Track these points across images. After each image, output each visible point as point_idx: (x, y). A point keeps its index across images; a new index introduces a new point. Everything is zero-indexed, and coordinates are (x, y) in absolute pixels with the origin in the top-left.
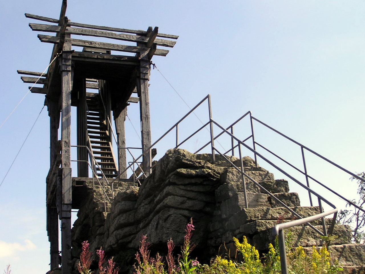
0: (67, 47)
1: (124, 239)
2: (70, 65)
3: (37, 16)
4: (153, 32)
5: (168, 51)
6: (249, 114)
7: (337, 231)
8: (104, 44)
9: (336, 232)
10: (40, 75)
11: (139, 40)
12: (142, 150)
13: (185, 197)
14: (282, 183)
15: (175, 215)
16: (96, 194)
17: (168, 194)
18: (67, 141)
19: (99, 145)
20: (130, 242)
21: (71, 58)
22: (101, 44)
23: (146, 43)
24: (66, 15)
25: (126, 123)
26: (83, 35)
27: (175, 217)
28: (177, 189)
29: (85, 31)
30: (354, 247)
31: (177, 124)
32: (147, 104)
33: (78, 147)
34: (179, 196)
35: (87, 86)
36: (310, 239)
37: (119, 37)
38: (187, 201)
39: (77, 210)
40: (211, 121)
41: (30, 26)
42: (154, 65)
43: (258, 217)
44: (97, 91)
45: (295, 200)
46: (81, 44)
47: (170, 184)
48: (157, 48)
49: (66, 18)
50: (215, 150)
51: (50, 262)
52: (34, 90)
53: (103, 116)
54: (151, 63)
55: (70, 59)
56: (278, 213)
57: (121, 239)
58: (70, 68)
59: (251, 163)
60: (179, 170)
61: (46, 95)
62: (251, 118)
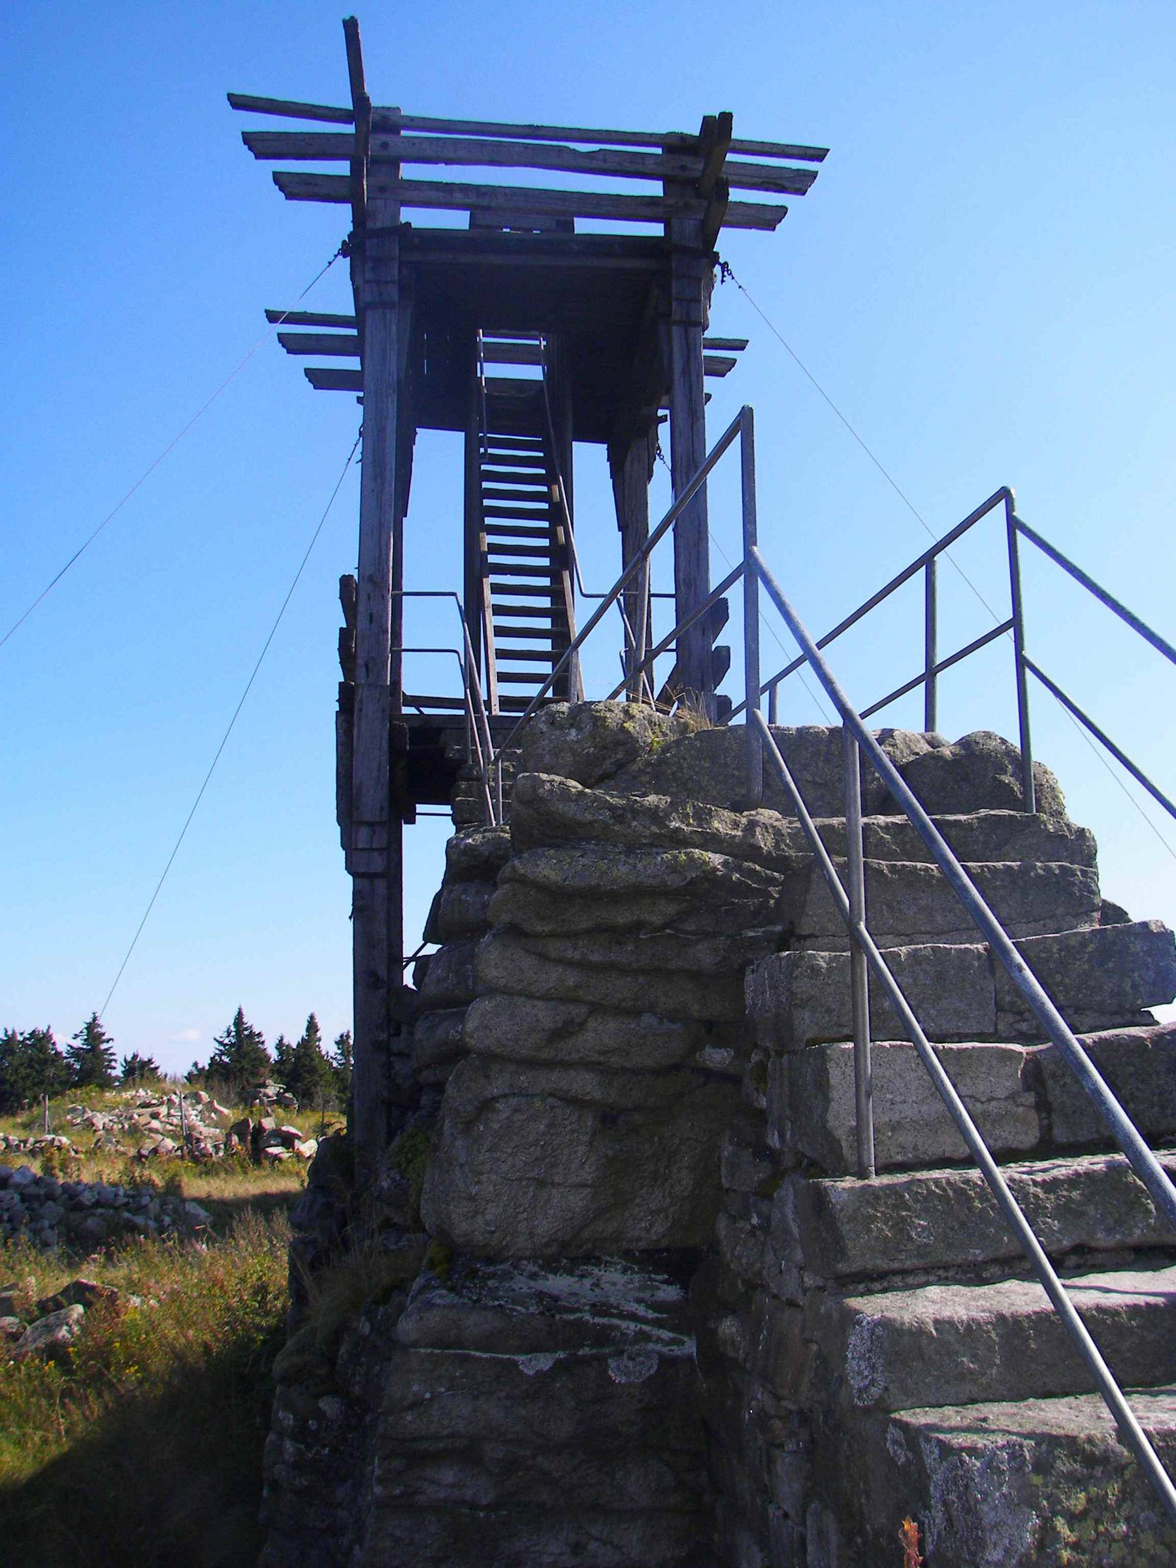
2: (392, 282)
5: (782, 211)
12: (674, 599)
13: (576, 1001)
14: (1137, 947)
15: (514, 1101)
26: (448, 162)
28: (528, 963)
34: (538, 998)
42: (724, 266)
48: (731, 198)
52: (320, 379)
62: (1014, 525)
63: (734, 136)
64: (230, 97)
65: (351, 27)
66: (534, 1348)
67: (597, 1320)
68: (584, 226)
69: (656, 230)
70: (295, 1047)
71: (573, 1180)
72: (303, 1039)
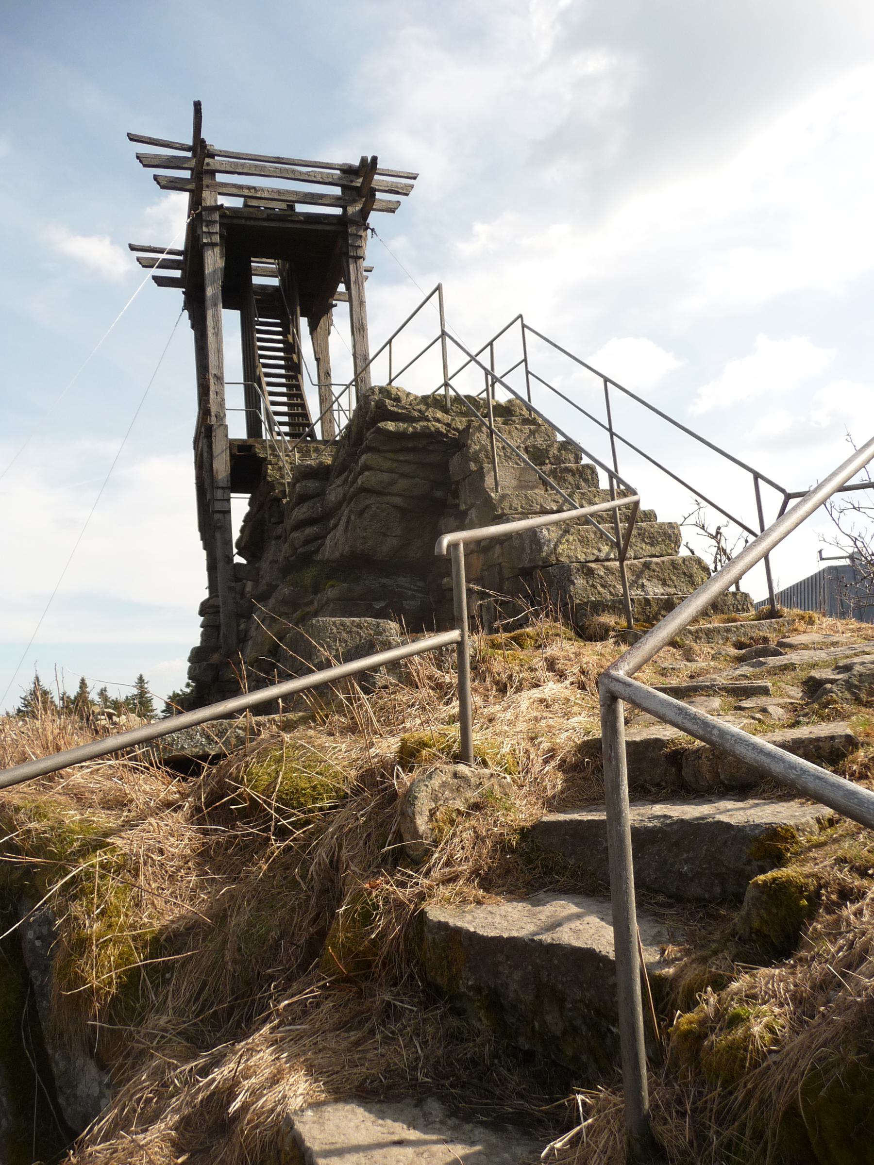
0: (209, 198)
1: (306, 547)
2: (217, 233)
3: (150, 138)
4: (369, 167)
6: (520, 320)
7: (655, 534)
8: (279, 192)
9: (652, 536)
10: (161, 251)
11: (344, 182)
15: (377, 505)
16: (273, 467)
17: (366, 468)
18: (219, 374)
19: (283, 380)
20: (317, 551)
21: (218, 218)
22: (273, 191)
23: (357, 187)
24: (203, 135)
25: (332, 339)
26: (239, 174)
27: (378, 508)
29: (243, 165)
30: (680, 562)
31: (390, 342)
32: (362, 303)
33: (245, 385)
35: (253, 272)
36: (602, 547)
37: (306, 178)
38: (400, 481)
39: (249, 495)
40: (444, 334)
41: (138, 158)
42: (373, 230)
43: (515, 508)
44: (275, 282)
45: (590, 477)
46: (235, 191)
47: (369, 449)
49: (203, 141)
50: (450, 389)
51: (206, 584)
52: (161, 281)
53: (288, 327)
54: (367, 228)
55: (216, 222)
56: (554, 501)
57: (301, 547)
58: (217, 239)
59: (522, 409)
60: (381, 425)
61: (184, 290)
62: (524, 326)
63: (378, 167)
64: (128, 134)
65: (197, 106)
66: (378, 600)
67: (399, 589)
68: (300, 208)
69: (338, 211)
70: (73, 699)
71: (394, 535)
72: (78, 693)
